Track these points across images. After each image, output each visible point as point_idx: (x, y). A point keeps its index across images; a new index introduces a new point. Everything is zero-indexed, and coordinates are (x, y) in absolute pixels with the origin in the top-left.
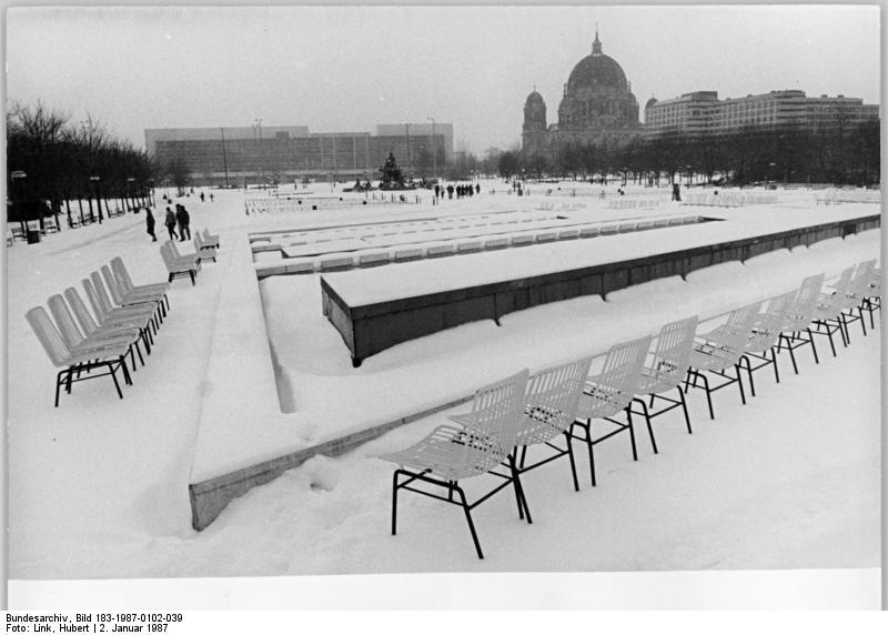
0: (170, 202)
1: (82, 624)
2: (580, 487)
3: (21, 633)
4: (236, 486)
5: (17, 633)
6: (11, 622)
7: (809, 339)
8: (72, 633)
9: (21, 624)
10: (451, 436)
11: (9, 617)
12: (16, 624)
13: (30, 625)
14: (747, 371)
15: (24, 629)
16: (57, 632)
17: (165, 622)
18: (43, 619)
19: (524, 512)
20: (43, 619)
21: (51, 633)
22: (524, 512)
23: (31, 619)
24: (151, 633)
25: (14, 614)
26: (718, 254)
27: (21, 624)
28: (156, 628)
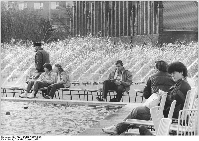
0: (192, 52)
1: (19, 139)
2: (130, 102)
3: (5, 140)
4: (41, 113)
5: (4, 140)
6: (3, 138)
7: (87, 92)
8: (18, 140)
9: (5, 138)
10: (119, 112)
11: (2, 137)
12: (4, 139)
13: (7, 139)
14: (99, 95)
15: (5, 140)
16: (14, 140)
17: (37, 138)
18: (10, 137)
19: (1, 92)
20: (10, 137)
21: (13, 140)
22: (1, 92)
23: (7, 137)
24: (34, 140)
25: (3, 136)
26: (13, 91)
27: (5, 138)
28: (36, 139)
